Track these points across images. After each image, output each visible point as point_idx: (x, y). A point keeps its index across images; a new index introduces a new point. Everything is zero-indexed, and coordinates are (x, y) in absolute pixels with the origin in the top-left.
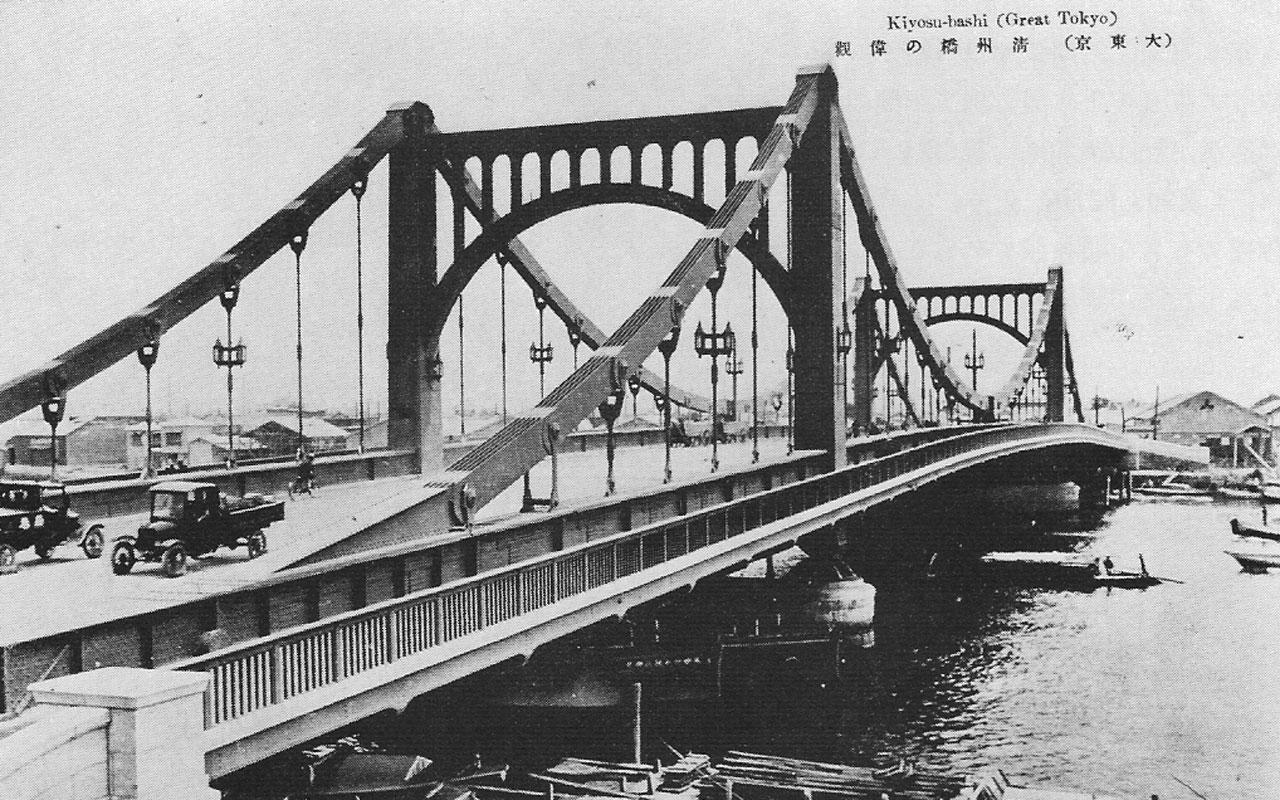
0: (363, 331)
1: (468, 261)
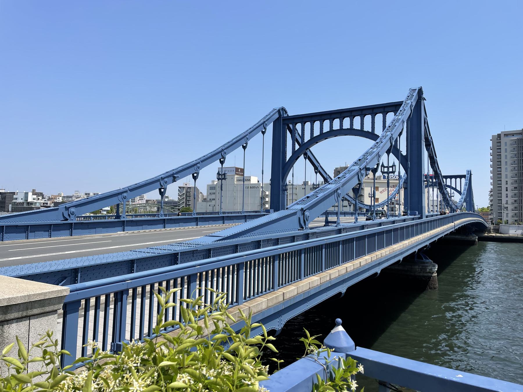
1: (295, 156)
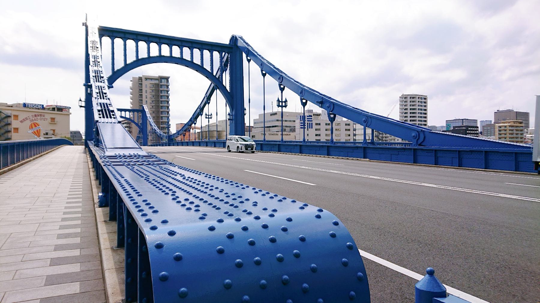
0: (249, 98)
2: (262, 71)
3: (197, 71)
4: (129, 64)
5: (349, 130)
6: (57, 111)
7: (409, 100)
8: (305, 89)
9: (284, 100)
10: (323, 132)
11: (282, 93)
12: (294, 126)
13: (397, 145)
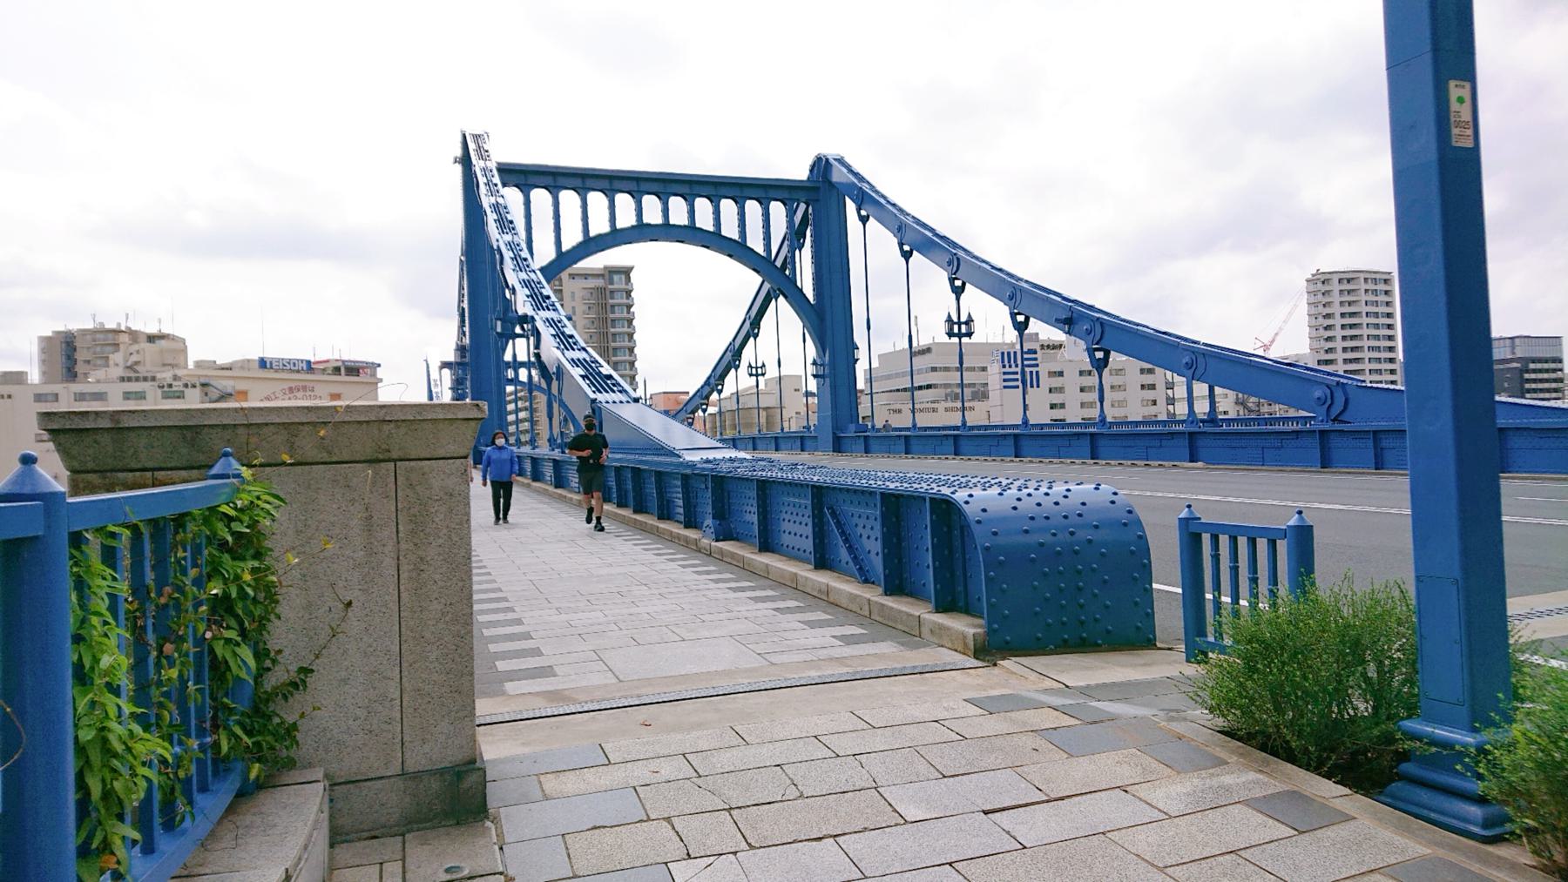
2: (901, 245)
3: (730, 256)
4: (568, 252)
5: (1152, 387)
6: (347, 375)
7: (1335, 287)
8: (1022, 290)
9: (963, 319)
10: (1072, 397)
11: (958, 299)
12: (986, 382)
13: (1290, 423)
